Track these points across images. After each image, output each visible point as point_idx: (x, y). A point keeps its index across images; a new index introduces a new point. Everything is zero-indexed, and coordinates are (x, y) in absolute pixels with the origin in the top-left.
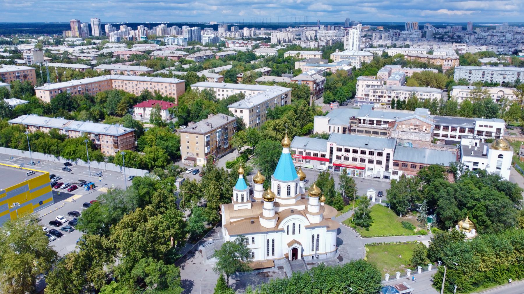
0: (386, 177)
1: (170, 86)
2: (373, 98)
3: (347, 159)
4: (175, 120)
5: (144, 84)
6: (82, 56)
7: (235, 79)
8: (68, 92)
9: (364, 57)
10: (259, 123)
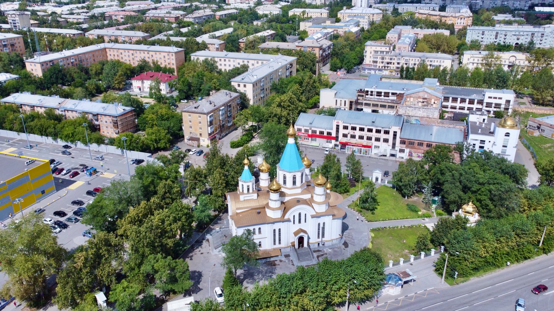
0: (393, 155)
1: (168, 55)
2: (381, 65)
3: (353, 137)
4: (175, 94)
5: (140, 53)
6: (72, 19)
7: (237, 45)
8: (61, 64)
9: (373, 15)
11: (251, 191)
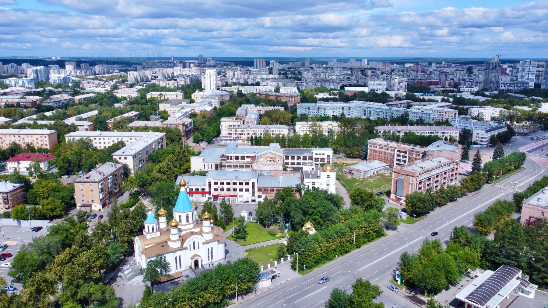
0: (253, 201)
2: (235, 136)
3: (222, 190)
4: (55, 170)
5: (10, 136)
7: (105, 125)
10: (142, 167)
11: (155, 230)
